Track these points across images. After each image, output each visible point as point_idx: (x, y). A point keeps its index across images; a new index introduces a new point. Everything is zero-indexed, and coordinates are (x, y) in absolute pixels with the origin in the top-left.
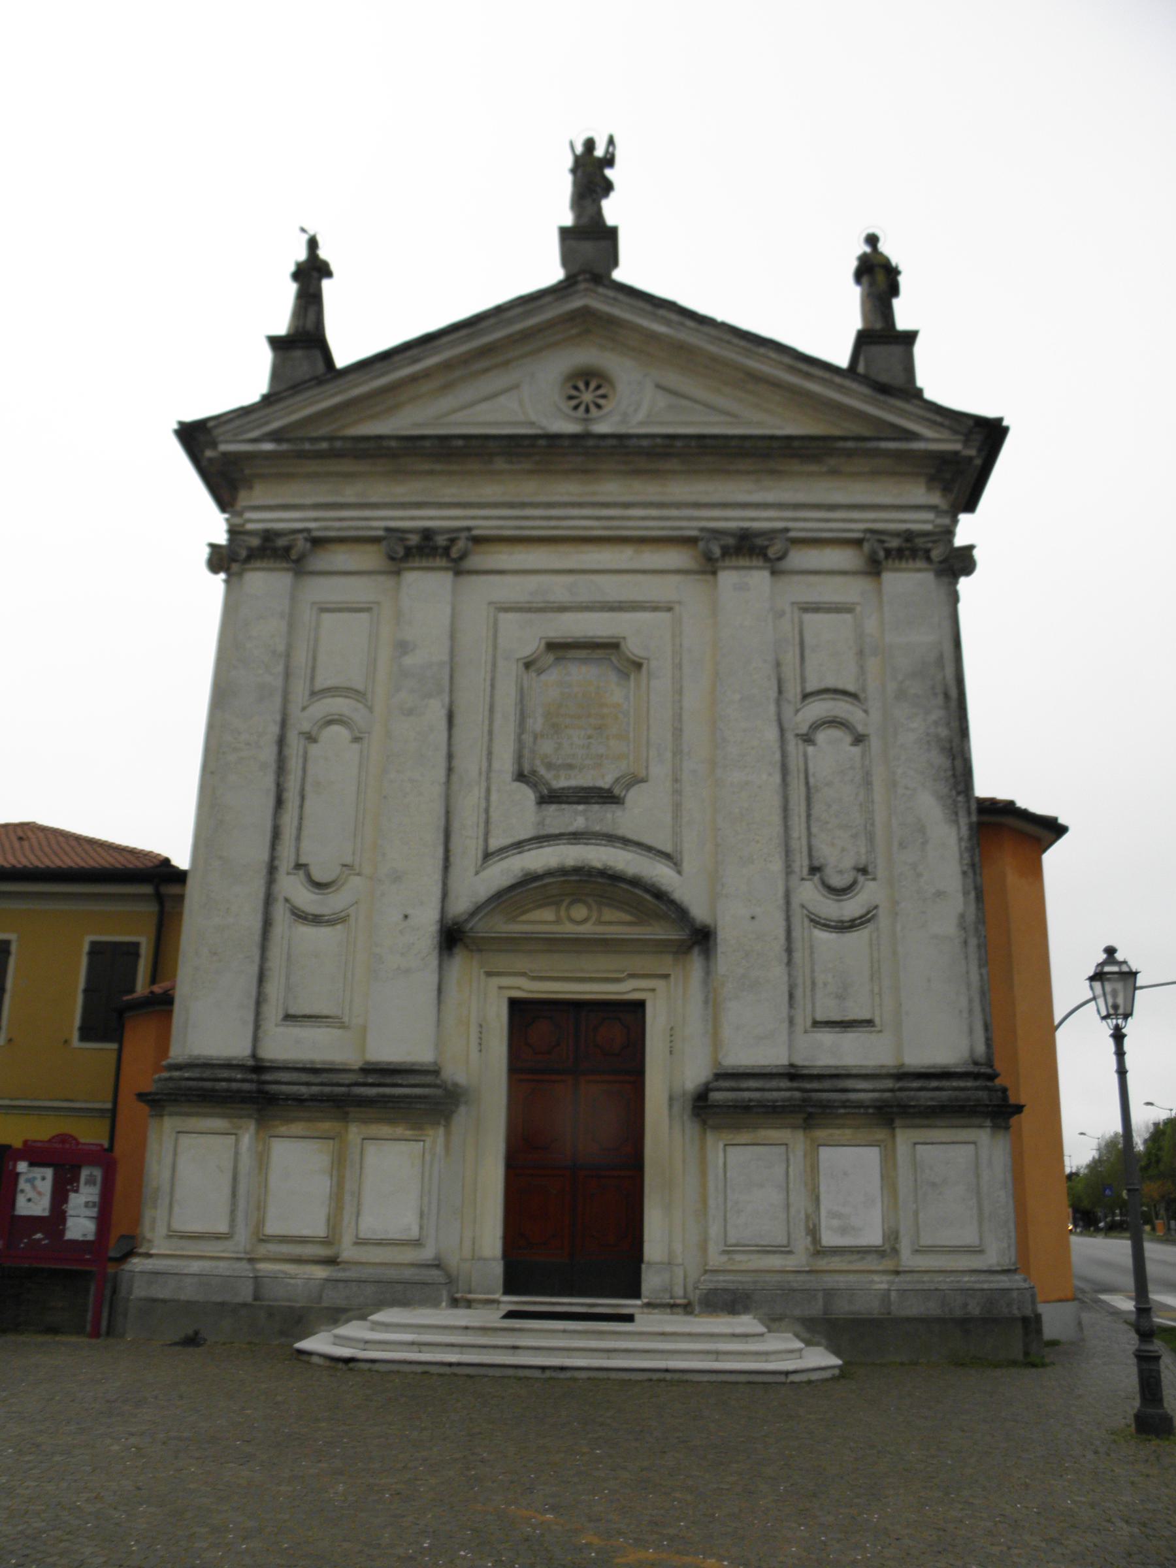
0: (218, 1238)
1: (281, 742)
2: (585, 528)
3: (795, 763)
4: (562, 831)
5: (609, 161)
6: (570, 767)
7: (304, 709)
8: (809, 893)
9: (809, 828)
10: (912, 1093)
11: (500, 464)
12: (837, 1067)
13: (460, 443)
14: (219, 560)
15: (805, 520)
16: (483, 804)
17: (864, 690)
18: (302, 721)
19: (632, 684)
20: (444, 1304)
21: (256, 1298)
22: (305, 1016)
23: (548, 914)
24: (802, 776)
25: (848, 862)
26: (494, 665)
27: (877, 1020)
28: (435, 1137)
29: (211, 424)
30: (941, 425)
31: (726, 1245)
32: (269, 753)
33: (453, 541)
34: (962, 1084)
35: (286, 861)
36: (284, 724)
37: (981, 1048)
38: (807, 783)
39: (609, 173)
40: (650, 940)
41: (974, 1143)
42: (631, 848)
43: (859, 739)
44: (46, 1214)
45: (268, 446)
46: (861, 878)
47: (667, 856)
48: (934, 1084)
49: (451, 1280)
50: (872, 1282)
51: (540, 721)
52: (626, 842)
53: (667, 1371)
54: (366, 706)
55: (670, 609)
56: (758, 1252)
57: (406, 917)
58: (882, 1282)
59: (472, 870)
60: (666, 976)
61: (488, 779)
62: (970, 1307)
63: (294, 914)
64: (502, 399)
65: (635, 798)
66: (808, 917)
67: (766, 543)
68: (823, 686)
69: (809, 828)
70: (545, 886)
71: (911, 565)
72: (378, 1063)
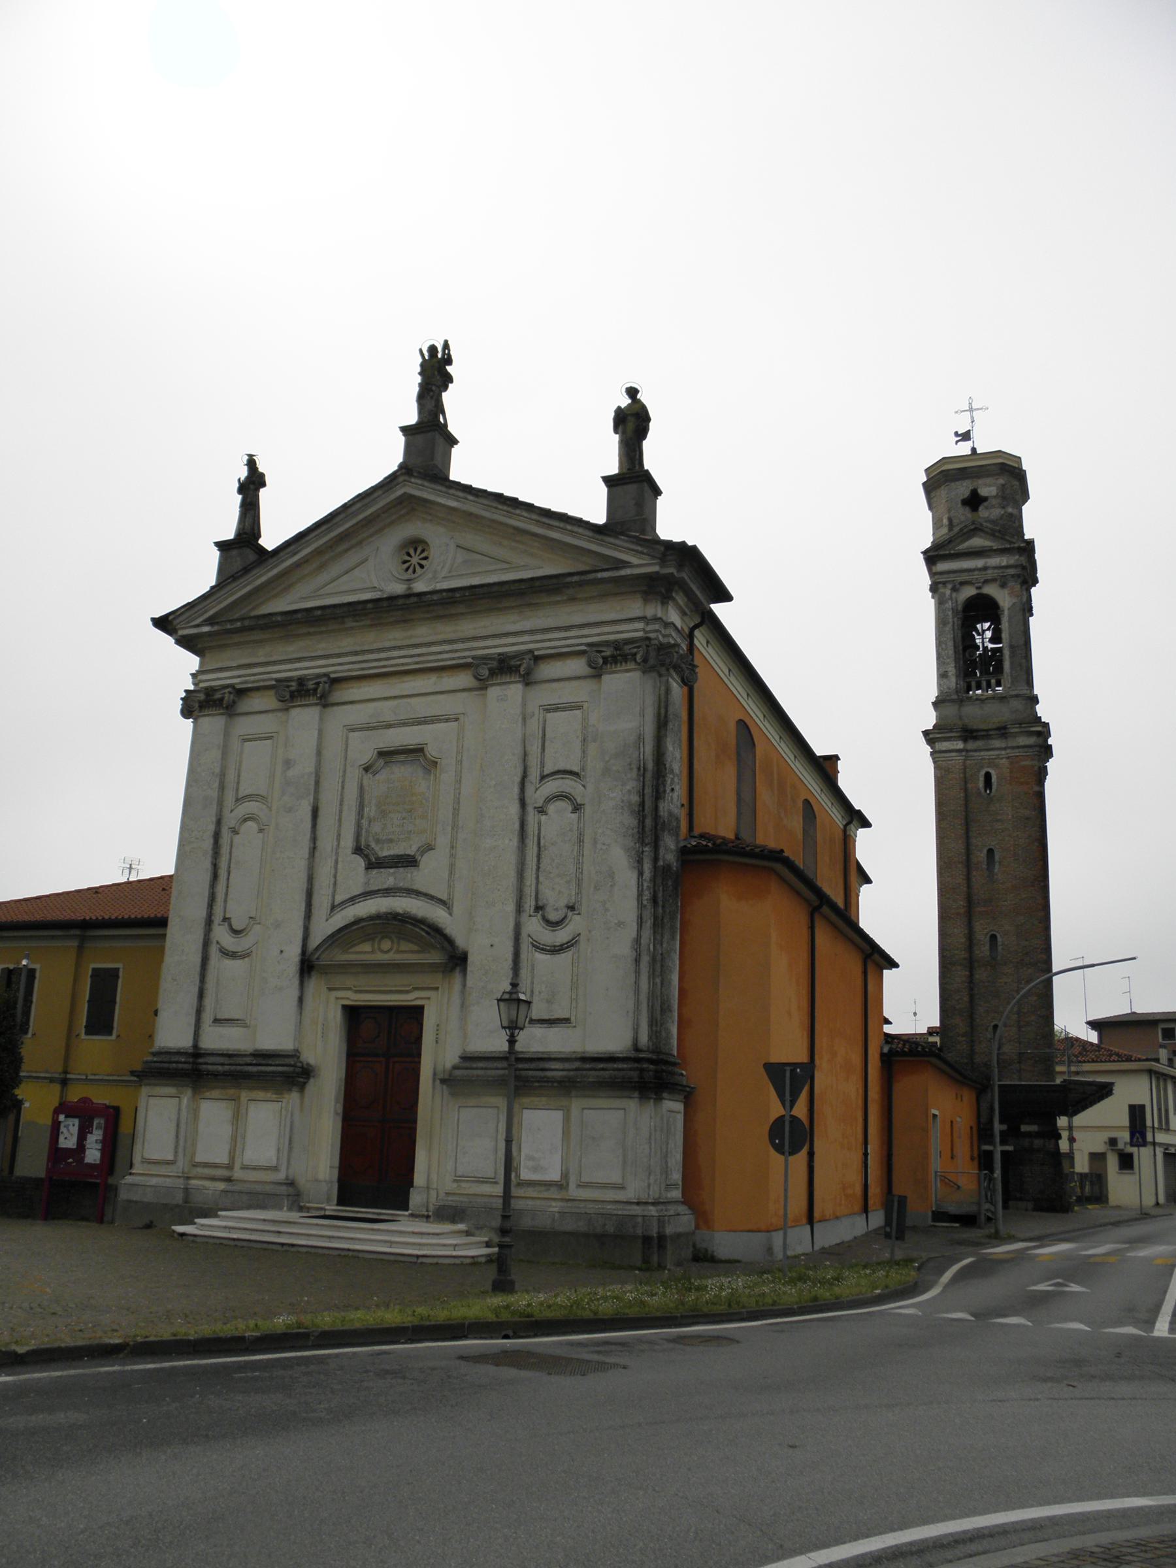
0: (168, 1164)
1: (217, 836)
2: (403, 664)
3: (531, 829)
4: (380, 888)
5: (448, 361)
6: (391, 841)
7: (232, 811)
8: (533, 926)
9: (537, 878)
10: (584, 1072)
11: (350, 623)
12: (543, 1053)
13: (319, 612)
14: (192, 706)
15: (550, 640)
16: (333, 872)
17: (583, 769)
18: (230, 820)
19: (432, 778)
20: (285, 1208)
21: (186, 1202)
22: (225, 1020)
23: (367, 947)
24: (536, 838)
25: (562, 902)
26: (345, 771)
27: (573, 1019)
28: (295, 1096)
29: (171, 618)
30: (642, 553)
31: (456, 1176)
32: (208, 844)
33: (318, 684)
34: (620, 1066)
35: (218, 917)
36: (219, 822)
37: (644, 1039)
38: (539, 843)
39: (449, 368)
40: (424, 964)
41: (624, 1109)
42: (422, 898)
43: (577, 808)
44: (75, 1147)
45: (206, 629)
46: (570, 914)
47: (442, 902)
48: (601, 1066)
49: (298, 1195)
50: (550, 1206)
51: (374, 808)
52: (418, 893)
53: (349, 1250)
54: (268, 807)
55: (457, 720)
56: (477, 1181)
57: (282, 952)
58: (556, 1207)
59: (324, 918)
60: (437, 989)
61: (337, 854)
62: (607, 1227)
63: (221, 951)
64: (356, 571)
65: (427, 862)
66: (532, 943)
67: (519, 663)
68: (556, 769)
69: (537, 878)
70: (362, 927)
71: (624, 667)
72: (261, 1050)
